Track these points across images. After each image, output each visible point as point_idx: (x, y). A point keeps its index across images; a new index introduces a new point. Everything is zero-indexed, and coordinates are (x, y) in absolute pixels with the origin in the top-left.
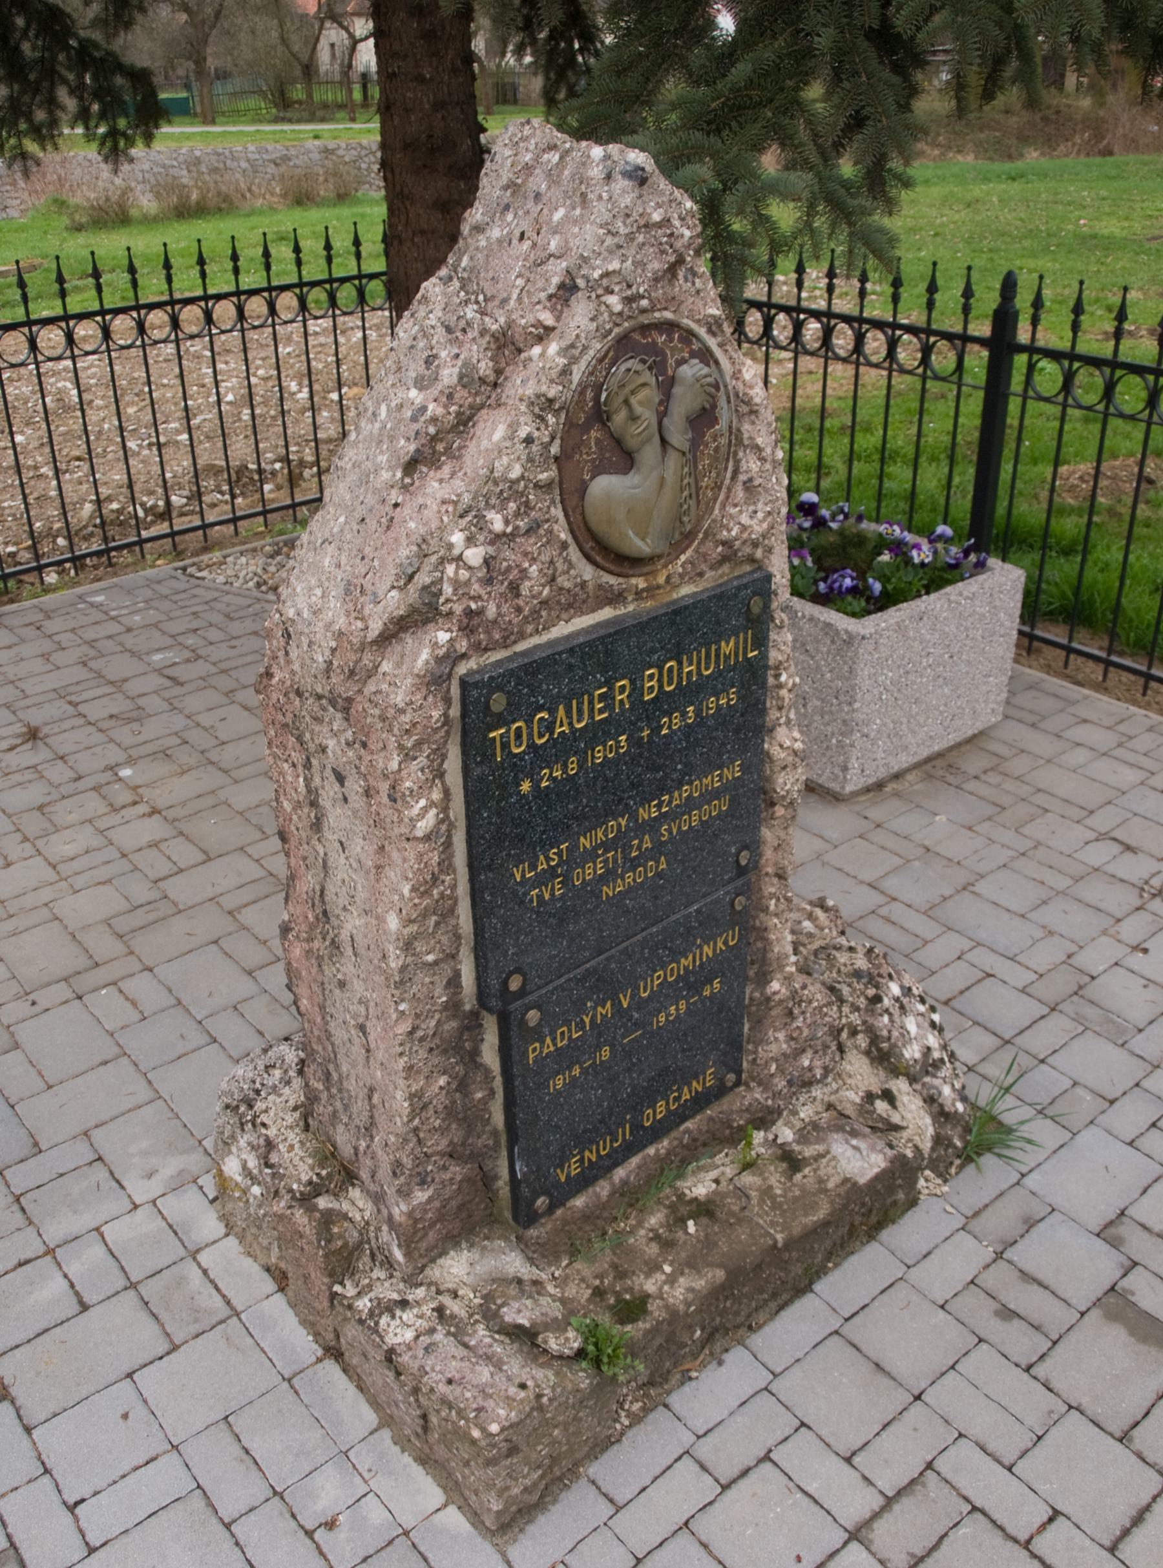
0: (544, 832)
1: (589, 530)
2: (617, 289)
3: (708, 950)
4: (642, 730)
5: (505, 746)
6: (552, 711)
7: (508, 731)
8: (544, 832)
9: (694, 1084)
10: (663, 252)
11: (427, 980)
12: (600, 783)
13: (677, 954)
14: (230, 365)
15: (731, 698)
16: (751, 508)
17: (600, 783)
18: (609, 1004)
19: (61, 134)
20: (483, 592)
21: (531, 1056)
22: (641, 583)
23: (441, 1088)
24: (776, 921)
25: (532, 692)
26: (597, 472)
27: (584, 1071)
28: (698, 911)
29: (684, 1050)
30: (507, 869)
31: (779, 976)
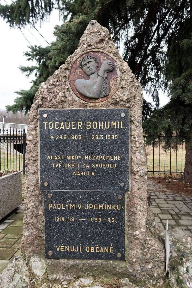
0: (57, 150)
1: (79, 92)
2: (86, 43)
3: (109, 207)
4: (86, 136)
5: (47, 126)
6: (60, 123)
7: (48, 123)
8: (57, 150)
9: (105, 248)
10: (98, 38)
11: (32, 177)
12: (73, 144)
13: (97, 202)
14: (168, 161)
15: (115, 137)
16: (124, 94)
17: (73, 144)
18: (74, 205)
19: (176, 148)
20: (47, 94)
21: (49, 207)
22: (92, 104)
23: (31, 205)
24: (140, 213)
25: (55, 116)
26: (79, 77)
27: (65, 220)
28: (105, 193)
29: (101, 235)
30: (46, 155)
31: (139, 230)
